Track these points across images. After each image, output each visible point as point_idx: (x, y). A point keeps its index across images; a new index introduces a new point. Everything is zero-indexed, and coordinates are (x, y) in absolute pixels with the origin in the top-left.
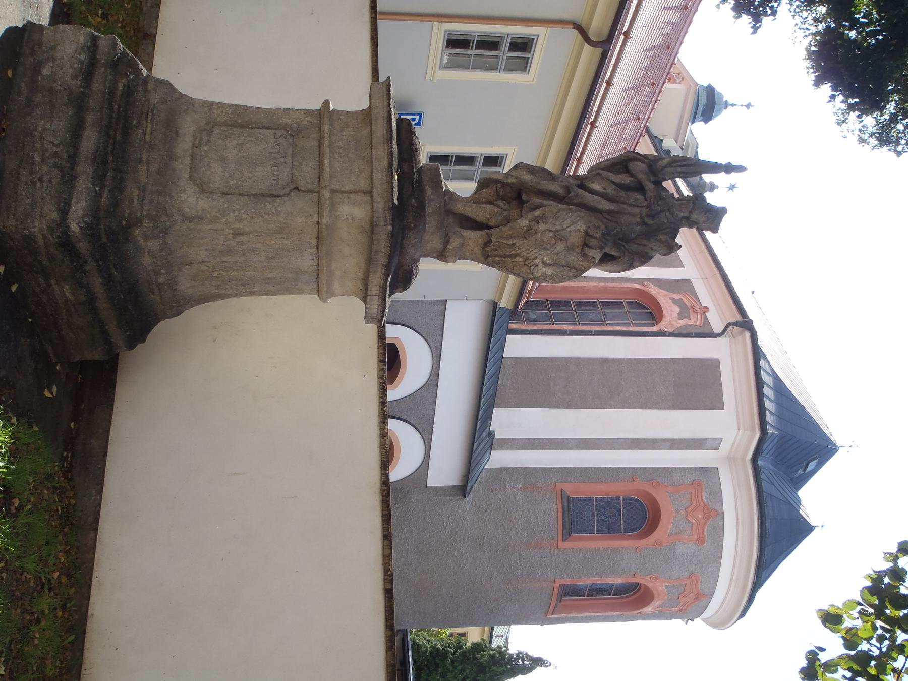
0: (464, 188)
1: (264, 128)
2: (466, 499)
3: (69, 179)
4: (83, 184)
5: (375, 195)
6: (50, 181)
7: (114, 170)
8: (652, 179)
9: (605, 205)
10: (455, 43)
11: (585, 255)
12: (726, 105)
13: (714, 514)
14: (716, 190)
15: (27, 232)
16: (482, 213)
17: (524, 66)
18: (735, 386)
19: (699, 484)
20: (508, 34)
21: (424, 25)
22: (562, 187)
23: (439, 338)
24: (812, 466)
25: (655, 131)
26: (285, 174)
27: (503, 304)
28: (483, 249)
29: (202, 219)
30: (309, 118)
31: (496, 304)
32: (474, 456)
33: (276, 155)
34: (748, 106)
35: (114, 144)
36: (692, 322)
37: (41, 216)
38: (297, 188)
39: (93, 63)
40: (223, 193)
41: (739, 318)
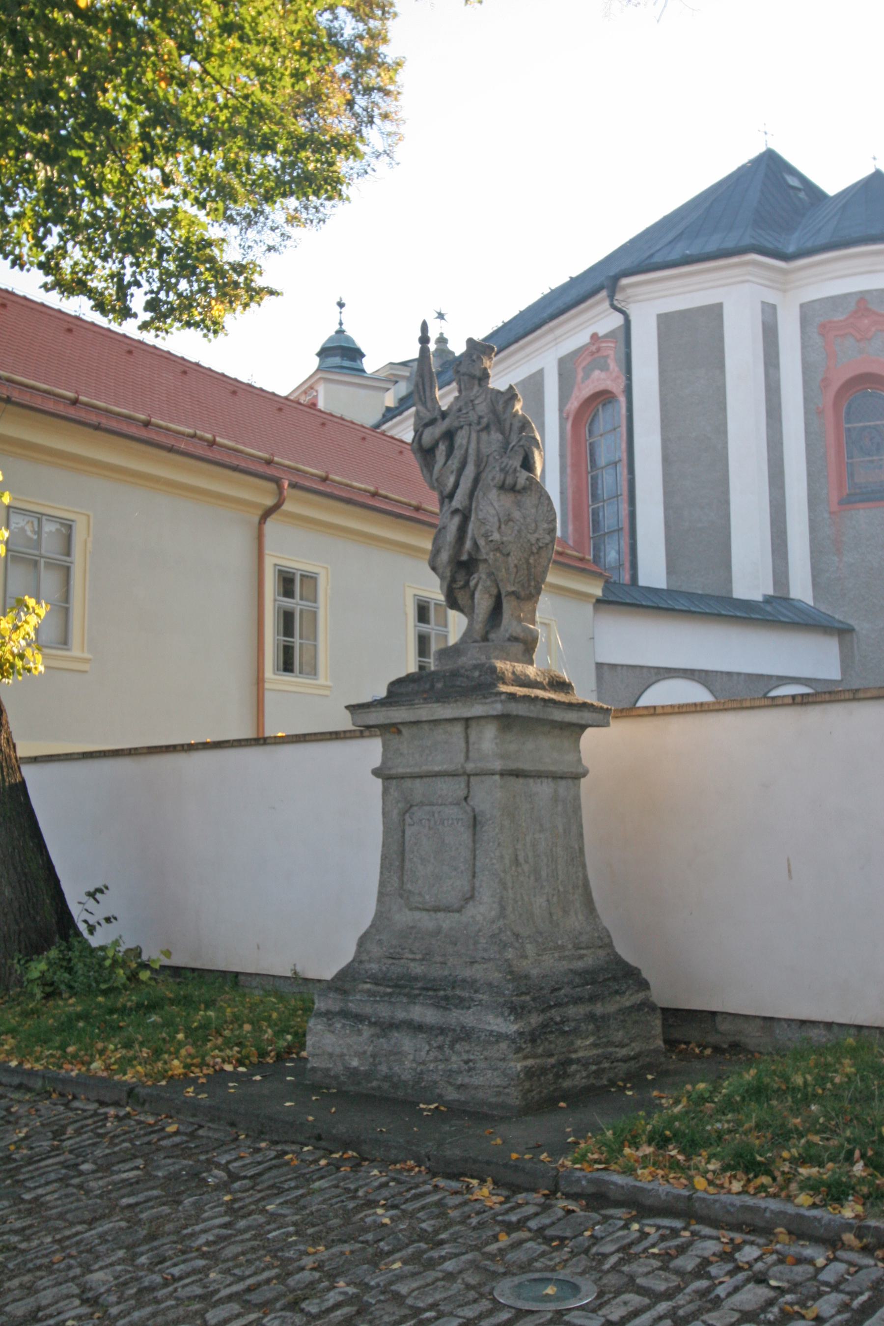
0: (456, 625)
1: (403, 836)
2: (857, 628)
3: (466, 1035)
4: (468, 1018)
5: (468, 714)
6: (468, 1052)
7: (453, 988)
8: (440, 421)
9: (470, 471)
10: (287, 666)
11: (525, 489)
12: (340, 332)
13: (862, 303)
14: (445, 336)
15: (522, 1075)
16: (483, 603)
17: (310, 579)
18: (690, 292)
19: (823, 326)
20: (275, 600)
21: (269, 698)
22: (452, 518)
23: (645, 671)
24: (793, 181)
25: (377, 417)
26: (452, 812)
27: (598, 592)
28: (523, 600)
29: (502, 897)
30: (392, 791)
31: (599, 601)
32: (797, 619)
33: (432, 822)
34: (341, 305)
35: (427, 989)
36: (611, 353)
37: (504, 1060)
38: (466, 799)
39: (344, 1014)
40: (474, 876)
41: (604, 294)
